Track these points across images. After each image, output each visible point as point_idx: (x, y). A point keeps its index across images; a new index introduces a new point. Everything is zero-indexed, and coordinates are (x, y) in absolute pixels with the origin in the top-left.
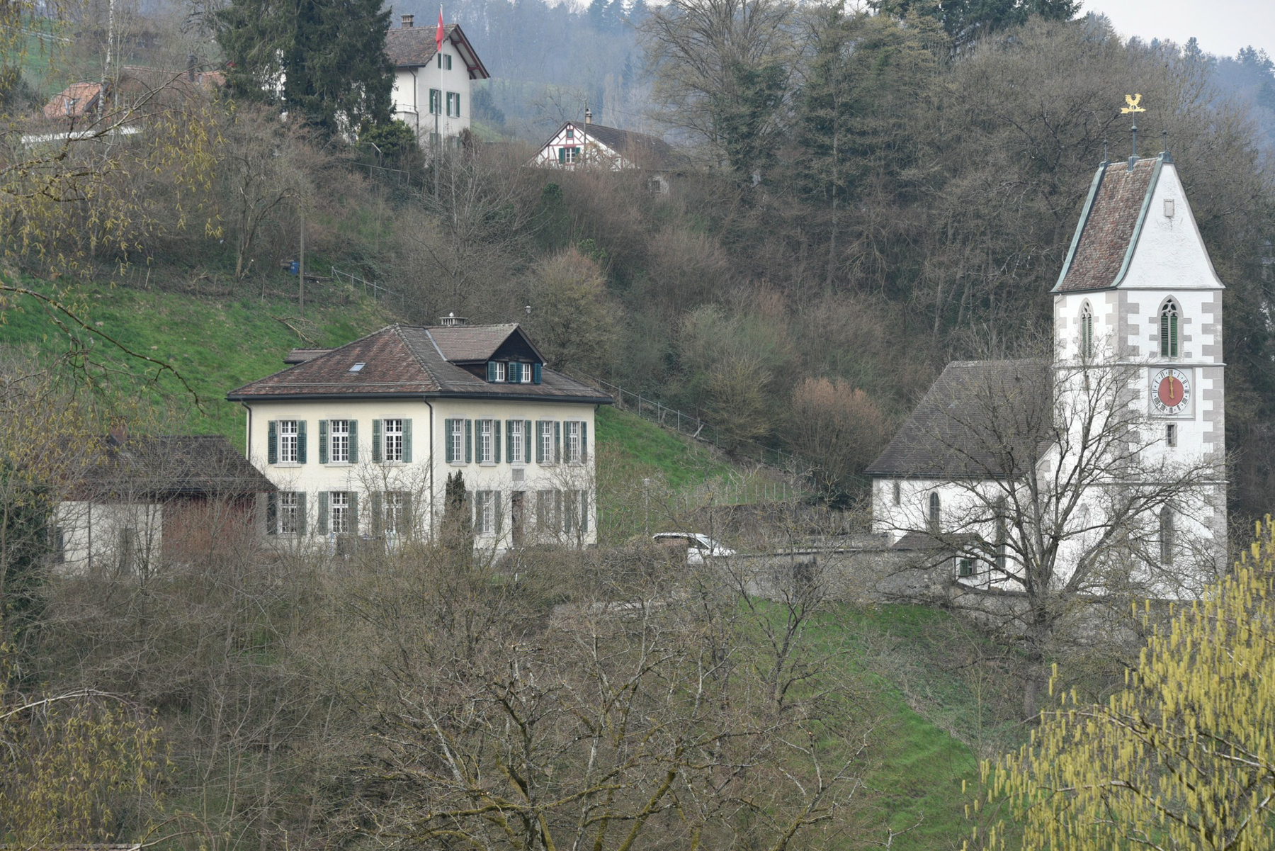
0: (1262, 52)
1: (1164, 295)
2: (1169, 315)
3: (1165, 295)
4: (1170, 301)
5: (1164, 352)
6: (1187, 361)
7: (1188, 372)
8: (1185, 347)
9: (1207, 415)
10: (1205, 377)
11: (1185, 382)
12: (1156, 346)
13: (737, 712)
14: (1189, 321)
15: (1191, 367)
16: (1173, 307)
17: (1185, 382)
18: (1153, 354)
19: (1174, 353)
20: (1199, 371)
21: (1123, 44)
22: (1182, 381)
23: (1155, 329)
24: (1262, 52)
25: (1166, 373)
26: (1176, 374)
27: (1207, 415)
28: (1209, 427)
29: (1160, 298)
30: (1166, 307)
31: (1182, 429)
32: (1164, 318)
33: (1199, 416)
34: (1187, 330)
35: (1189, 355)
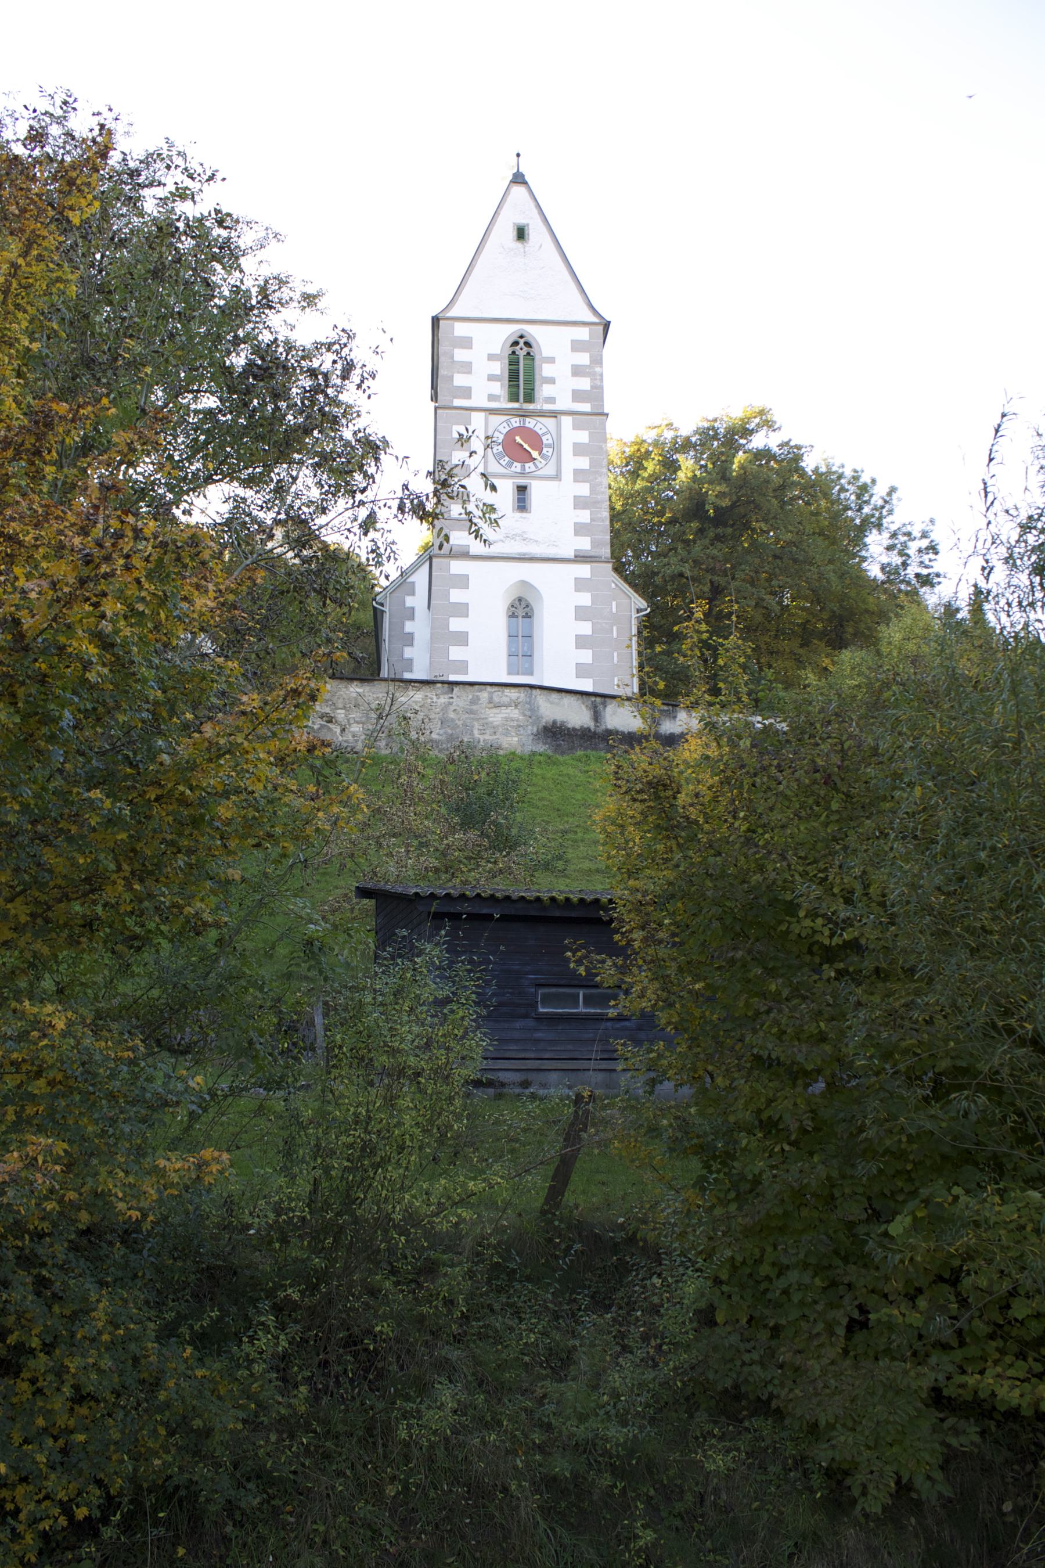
0: (899, 500)
1: (509, 331)
2: (522, 354)
3: (512, 329)
4: (521, 337)
5: (514, 397)
6: (547, 407)
7: (550, 422)
8: (544, 391)
9: (579, 475)
10: (576, 427)
11: (544, 434)
12: (499, 388)
13: (23, 689)
14: (551, 360)
15: (554, 414)
16: (527, 344)
17: (544, 434)
18: (492, 398)
19: (530, 398)
20: (567, 421)
21: (642, 726)
22: (540, 432)
23: (499, 368)
24: (899, 500)
25: (516, 422)
26: (530, 423)
27: (579, 475)
28: (584, 490)
29: (506, 332)
30: (516, 343)
31: (537, 490)
32: (513, 361)
33: (567, 474)
34: (546, 370)
35: (552, 400)
